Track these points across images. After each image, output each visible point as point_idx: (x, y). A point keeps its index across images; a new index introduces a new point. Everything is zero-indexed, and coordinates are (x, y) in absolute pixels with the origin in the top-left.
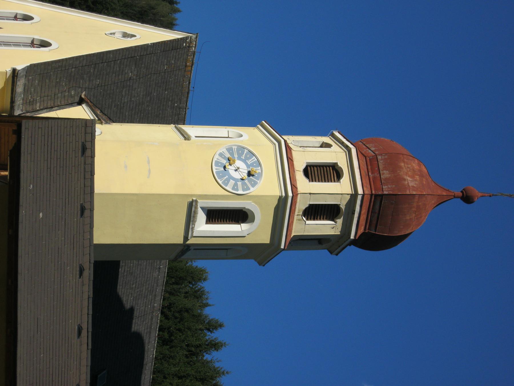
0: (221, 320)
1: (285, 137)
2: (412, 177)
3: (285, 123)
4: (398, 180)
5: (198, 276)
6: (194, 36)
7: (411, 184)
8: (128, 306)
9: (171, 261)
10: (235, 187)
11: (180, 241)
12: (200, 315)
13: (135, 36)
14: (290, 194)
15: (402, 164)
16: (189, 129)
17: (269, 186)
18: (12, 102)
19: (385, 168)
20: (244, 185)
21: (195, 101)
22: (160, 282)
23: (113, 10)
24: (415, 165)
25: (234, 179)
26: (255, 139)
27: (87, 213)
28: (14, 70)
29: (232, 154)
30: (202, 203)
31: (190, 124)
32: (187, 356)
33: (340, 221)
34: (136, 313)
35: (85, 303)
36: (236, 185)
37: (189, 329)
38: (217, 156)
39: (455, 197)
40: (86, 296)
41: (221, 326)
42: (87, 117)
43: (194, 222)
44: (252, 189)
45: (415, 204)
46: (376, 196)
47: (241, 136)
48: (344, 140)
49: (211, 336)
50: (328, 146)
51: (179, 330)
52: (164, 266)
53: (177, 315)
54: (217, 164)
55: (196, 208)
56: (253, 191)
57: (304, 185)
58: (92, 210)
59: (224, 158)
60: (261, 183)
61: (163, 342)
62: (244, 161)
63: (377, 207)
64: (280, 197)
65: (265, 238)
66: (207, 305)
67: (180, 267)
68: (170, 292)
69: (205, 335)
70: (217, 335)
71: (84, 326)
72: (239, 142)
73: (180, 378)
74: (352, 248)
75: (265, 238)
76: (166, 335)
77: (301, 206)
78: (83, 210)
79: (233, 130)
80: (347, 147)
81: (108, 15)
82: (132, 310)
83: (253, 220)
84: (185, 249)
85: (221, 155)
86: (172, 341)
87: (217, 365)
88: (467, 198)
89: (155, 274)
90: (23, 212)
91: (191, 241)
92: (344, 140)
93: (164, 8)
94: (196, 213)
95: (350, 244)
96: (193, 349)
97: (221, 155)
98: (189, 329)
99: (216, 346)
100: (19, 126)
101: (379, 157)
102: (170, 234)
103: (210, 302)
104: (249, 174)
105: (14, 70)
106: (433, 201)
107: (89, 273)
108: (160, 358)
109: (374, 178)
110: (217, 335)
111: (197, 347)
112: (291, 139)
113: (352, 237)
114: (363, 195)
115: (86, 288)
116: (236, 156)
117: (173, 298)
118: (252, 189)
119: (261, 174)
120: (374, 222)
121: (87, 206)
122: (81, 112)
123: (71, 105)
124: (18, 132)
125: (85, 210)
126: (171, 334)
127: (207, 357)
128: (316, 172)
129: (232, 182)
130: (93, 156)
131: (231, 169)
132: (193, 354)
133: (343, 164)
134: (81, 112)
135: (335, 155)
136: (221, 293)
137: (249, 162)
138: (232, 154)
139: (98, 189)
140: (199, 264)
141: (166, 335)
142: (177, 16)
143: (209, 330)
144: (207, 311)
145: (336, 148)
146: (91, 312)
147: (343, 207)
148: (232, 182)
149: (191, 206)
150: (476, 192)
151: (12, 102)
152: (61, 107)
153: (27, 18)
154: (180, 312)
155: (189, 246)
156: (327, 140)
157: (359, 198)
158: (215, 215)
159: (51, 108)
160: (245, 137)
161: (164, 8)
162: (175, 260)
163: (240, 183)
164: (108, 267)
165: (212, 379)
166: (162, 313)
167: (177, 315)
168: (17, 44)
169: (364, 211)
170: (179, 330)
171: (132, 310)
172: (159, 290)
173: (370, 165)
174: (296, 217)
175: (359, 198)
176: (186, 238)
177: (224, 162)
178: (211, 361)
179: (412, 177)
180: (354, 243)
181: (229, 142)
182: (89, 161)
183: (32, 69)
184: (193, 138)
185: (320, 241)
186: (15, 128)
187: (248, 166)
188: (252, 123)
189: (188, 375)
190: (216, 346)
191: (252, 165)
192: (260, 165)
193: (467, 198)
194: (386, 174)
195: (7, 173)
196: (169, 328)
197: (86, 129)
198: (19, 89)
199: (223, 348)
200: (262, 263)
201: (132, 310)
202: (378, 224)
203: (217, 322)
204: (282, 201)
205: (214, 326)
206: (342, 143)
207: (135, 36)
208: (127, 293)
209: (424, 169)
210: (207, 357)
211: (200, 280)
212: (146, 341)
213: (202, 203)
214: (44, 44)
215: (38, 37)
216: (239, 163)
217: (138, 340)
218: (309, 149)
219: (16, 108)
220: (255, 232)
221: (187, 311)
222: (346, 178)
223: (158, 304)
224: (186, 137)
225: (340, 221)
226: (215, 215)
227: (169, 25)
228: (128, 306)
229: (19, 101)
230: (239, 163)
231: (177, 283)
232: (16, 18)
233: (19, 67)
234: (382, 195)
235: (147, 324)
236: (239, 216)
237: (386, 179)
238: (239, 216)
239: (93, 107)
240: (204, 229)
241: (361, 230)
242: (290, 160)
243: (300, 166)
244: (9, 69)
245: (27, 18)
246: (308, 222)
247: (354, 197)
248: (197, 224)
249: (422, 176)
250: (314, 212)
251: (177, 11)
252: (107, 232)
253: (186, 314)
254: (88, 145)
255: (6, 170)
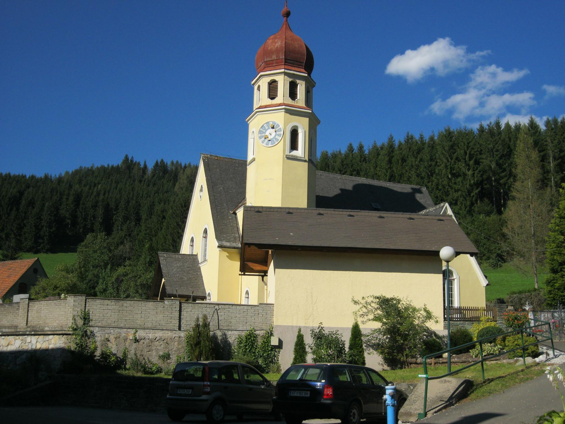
0: (348, 145)
1: (254, 109)
2: (276, 43)
3: (246, 108)
4: (277, 51)
5: (325, 156)
6: (202, 155)
7: (280, 44)
8: (339, 192)
9: (317, 169)
10: (279, 135)
11: (306, 164)
12: (345, 155)
13: (192, 238)
14: (284, 107)
15: (269, 48)
16: (249, 159)
17: (279, 118)
18: (234, 248)
19: (271, 57)
20: (278, 131)
21: (236, 156)
22: (327, 175)
23: (189, 197)
24: (270, 42)
25: (275, 136)
26: (255, 124)
27: (291, 211)
28: (218, 247)
29: (262, 137)
30: (287, 153)
31: (247, 158)
32: (366, 163)
33: (298, 81)
34: (343, 187)
35: (337, 212)
36: (278, 135)
37: (351, 161)
38: (264, 144)
39: (287, 21)
40: (333, 212)
41: (351, 145)
42: (243, 210)
43: (297, 157)
44: (281, 127)
45: (290, 42)
46: (285, 62)
47: (253, 132)
48: (256, 78)
49: (356, 150)
50: (259, 87)
51: (352, 166)
52: (320, 173)
53: (345, 167)
54: (267, 144)
55: (290, 155)
56: (282, 126)
57: (279, 99)
58: (289, 208)
59: (264, 141)
60: (277, 122)
61: (358, 174)
62: (266, 130)
63: (291, 62)
64: (285, 112)
65: (306, 120)
66: (340, 152)
67: (319, 164)
68: (333, 170)
69: (355, 153)
70: (356, 147)
71: (348, 213)
72: (256, 133)
73: (377, 166)
74: (313, 75)
75: (306, 120)
76: (355, 173)
77: (290, 101)
78: (289, 213)
79: (250, 136)
80: (260, 77)
81: (191, 199)
82: (341, 190)
83: (297, 127)
84: (310, 161)
85: (263, 142)
86: (358, 170)
87: (371, 147)
88: (288, 14)
89: (323, 177)
90: (290, 243)
91: (307, 159)
92: (256, 78)
93: (188, 171)
94: (292, 156)
95: (310, 77)
96: (362, 159)
97: (263, 142)
98: (351, 161)
99: (361, 147)
100: (246, 244)
101: (265, 60)
102: (303, 169)
103: (338, 150)
104: (273, 128)
105: (218, 247)
106: (289, 33)
107: (322, 211)
108: (366, 176)
109: (276, 63)
110: (356, 147)
111: (361, 157)
112: (255, 106)
113: (306, 75)
114: (285, 69)
115: (329, 212)
116: (263, 135)
117: (336, 169)
118: (281, 127)
119: (273, 122)
120: (299, 63)
121: (287, 211)
122: (240, 213)
123: (236, 218)
124: (249, 245)
125: (289, 212)
126: (354, 170)
127: (367, 152)
128: (272, 94)
129: (277, 137)
130: (262, 207)
131: (270, 137)
132: (365, 159)
133: (269, 79)
134: (240, 213)
135: (264, 83)
136: (334, 144)
137: (267, 128)
138: (262, 137)
139: (277, 203)
140: (319, 155)
141: (355, 173)
142: (192, 165)
143: (353, 151)
144: (343, 152)
145: (260, 83)
146: (341, 210)
147: (291, 80)
148: (277, 137)
149: (289, 158)
150: (284, 10)
151: (234, 248)
152: (237, 224)
153: (192, 240)
154: (343, 165)
155: (309, 160)
156: (256, 87)
157: (286, 71)
158: (294, 146)
159: (238, 229)
160: (254, 130)
161: (188, 171)
162: (315, 166)
163: (278, 133)
164: (320, 201)
165: (377, 150)
166: (343, 174)
167: (345, 167)
168: (206, 245)
169: (293, 68)
170: (352, 166)
171: (341, 190)
172: (332, 175)
173: (269, 65)
174: (296, 104)
175: (286, 71)
176: (305, 161)
177: (266, 140)
178: (369, 150)
179: (276, 43)
180: (309, 74)
181: (257, 138)
182: (265, 210)
183: (218, 238)
184: (254, 156)
185: (308, 92)
186: (247, 246)
187: (269, 128)
188: (246, 127)
189: (376, 162)
190: (361, 147)
191: (268, 127)
192: (268, 122)
193: (288, 14)
194: (274, 57)
195: (270, 251)
196: (351, 171)
197: (249, 210)
198: (228, 244)
199: (363, 144)
200: (319, 122)
201: (341, 190)
202: (300, 61)
203: (349, 147)
204: (287, 111)
205: (351, 149)
206: (258, 79)
207: (192, 238)
208: (333, 192)
209: (272, 37)
210: (367, 152)
211: (327, 155)
212: (357, 183)
213: (287, 153)
214: (206, 231)
215: (202, 234)
216: (267, 133)
217: (357, 187)
218: (261, 97)
219: (237, 246)
220: (303, 125)
221: (342, 162)
222: (276, 78)
223: (338, 176)
224: (254, 160)
225: (298, 81)
226: (294, 146)
227: (197, 168)
228: (339, 192)
229: (234, 245)
230: (267, 133)
231: (329, 167)
232: (192, 246)
233: (217, 244)
234: (285, 59)
235: (349, 182)
236: (294, 133)
237: (277, 57)
238: (294, 133)
239: (237, 207)
240: (301, 152)
241: (304, 71)
242: (266, 107)
243: (269, 102)
244: (218, 249)
245: (192, 240)
246: (298, 98)
247: (285, 74)
248: (298, 155)
249: (275, 38)
250: (293, 94)
251: (190, 165)
252: (301, 200)
253: (345, 162)
254: (257, 210)
255: (268, 251)
